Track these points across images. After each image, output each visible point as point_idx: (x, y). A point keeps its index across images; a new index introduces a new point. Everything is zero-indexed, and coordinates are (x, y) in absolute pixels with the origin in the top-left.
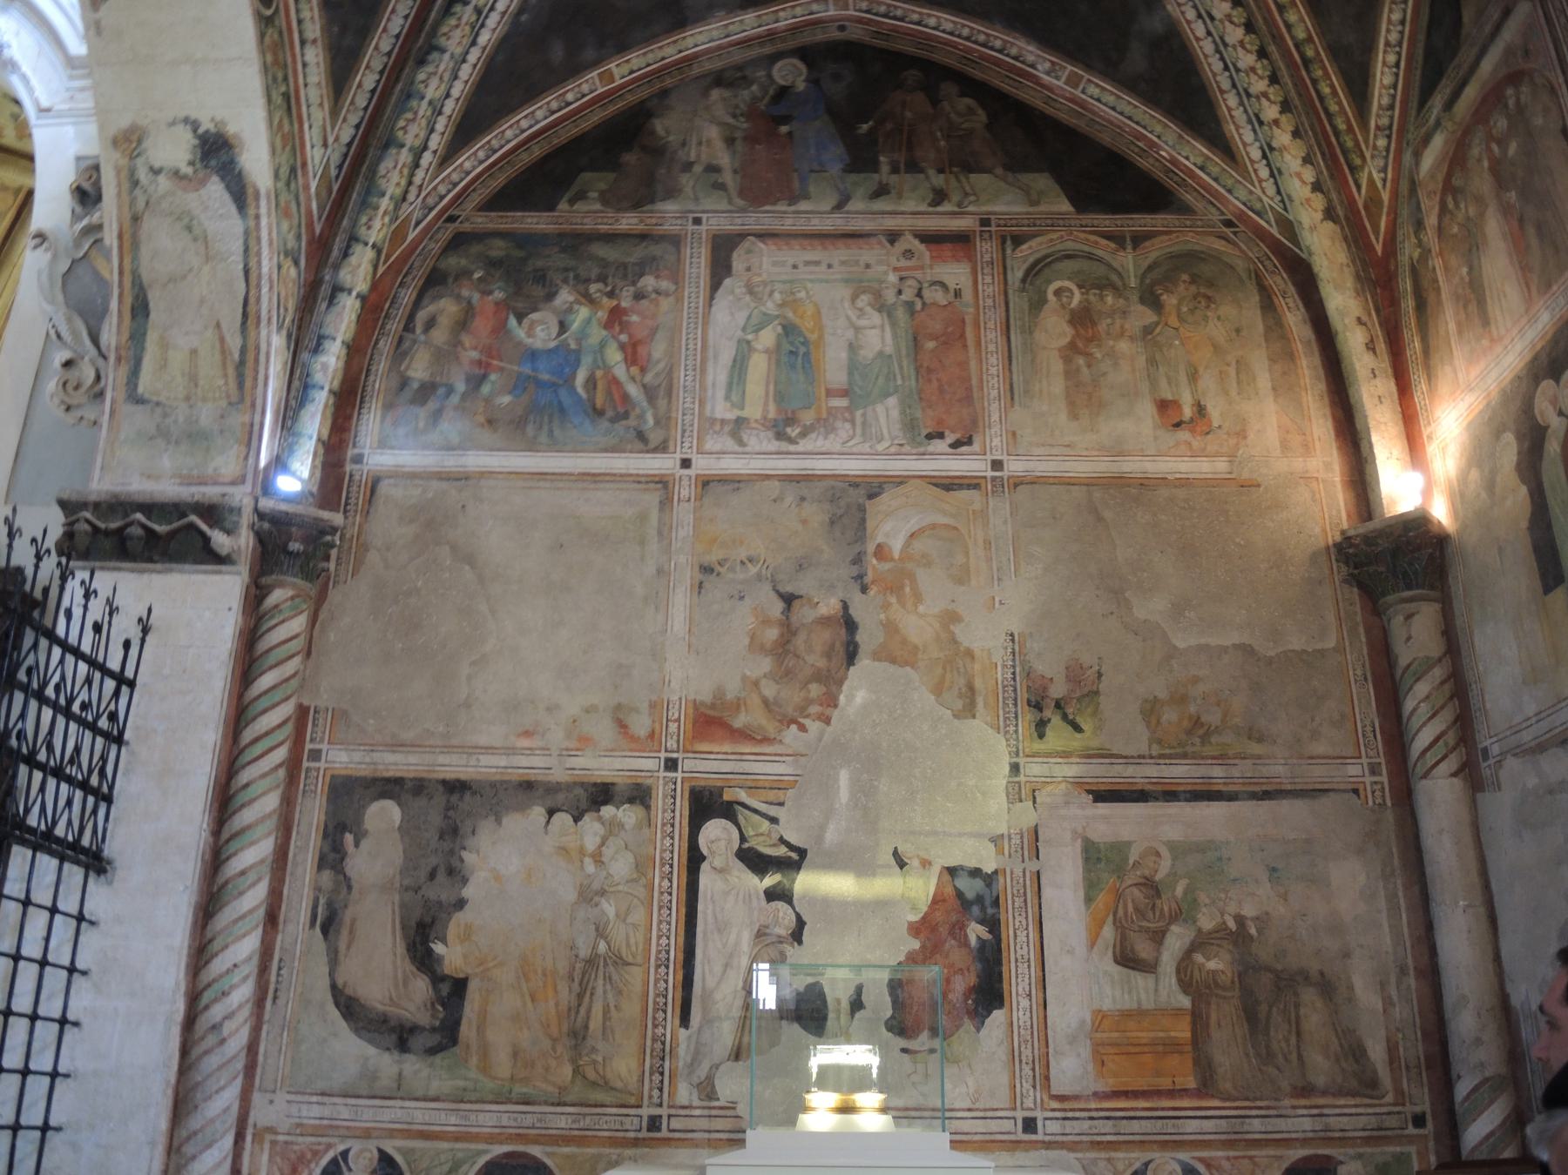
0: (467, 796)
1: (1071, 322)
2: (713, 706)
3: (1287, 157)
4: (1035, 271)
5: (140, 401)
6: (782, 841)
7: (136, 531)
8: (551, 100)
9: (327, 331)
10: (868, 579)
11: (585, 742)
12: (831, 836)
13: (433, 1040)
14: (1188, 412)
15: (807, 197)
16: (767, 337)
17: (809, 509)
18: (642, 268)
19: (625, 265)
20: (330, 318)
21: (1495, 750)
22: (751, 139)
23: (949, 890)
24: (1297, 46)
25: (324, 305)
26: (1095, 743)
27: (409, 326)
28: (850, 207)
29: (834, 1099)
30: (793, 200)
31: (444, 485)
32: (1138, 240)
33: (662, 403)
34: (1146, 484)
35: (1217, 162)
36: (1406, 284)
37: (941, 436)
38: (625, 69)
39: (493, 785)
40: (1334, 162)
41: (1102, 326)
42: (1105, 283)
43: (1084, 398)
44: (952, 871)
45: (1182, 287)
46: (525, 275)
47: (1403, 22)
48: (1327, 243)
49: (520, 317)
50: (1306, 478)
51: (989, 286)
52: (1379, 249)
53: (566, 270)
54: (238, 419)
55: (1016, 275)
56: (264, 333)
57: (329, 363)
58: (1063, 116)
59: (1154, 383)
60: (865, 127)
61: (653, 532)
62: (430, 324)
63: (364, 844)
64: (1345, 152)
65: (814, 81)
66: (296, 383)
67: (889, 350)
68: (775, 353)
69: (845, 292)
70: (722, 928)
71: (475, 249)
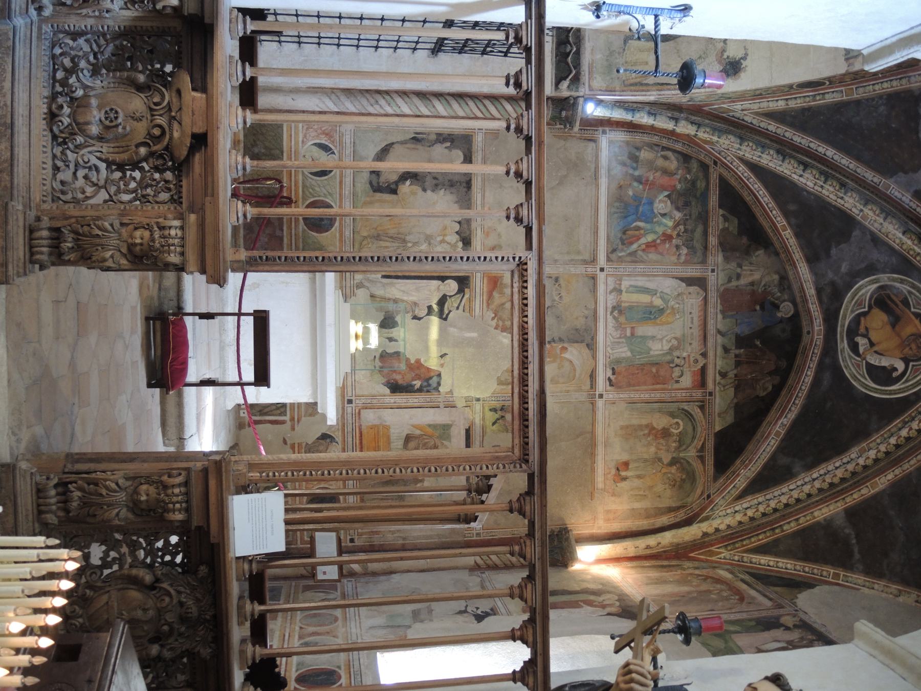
0: (465, 190)
1: (664, 428)
2: (501, 284)
3: (730, 519)
4: (688, 415)
5: (625, 42)
6: (450, 311)
7: (568, 49)
8: (772, 204)
9: (658, 117)
10: (554, 345)
11: (487, 235)
12: (452, 330)
13: (375, 184)
14: (623, 474)
15: (724, 318)
16: (658, 302)
17: (582, 321)
18: (691, 248)
19: (692, 240)
20: (664, 118)
21: (484, 575)
22: (753, 293)
23: (432, 374)
24: (780, 526)
25: (669, 115)
26: (488, 430)
27: (665, 148)
28: (719, 336)
29: (360, 333)
30: (722, 312)
31: (593, 170)
32: (702, 458)
33: (629, 259)
34: (593, 455)
35: (736, 493)
36: (674, 563)
37: (614, 374)
38: (788, 236)
39: (470, 199)
40: (730, 537)
41: (662, 441)
42: (681, 442)
43: (629, 432)
44: (439, 375)
45: (679, 475)
46: (688, 198)
47: (786, 568)
48: (693, 532)
49: (668, 196)
50: (595, 519)
51: (680, 395)
52: (692, 555)
53: (690, 215)
54: (617, 85)
55: (686, 406)
56: (655, 93)
57: (644, 119)
58: (761, 429)
59: (636, 461)
60: (758, 343)
61: (573, 257)
62: (666, 158)
63: (446, 151)
64: (734, 543)
65: (781, 321)
66: (635, 105)
67: (652, 353)
68: (651, 305)
69: (678, 334)
70: (418, 289)
71: (701, 175)
